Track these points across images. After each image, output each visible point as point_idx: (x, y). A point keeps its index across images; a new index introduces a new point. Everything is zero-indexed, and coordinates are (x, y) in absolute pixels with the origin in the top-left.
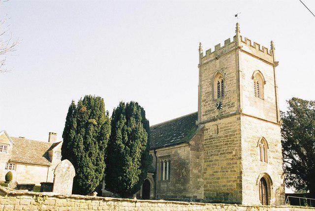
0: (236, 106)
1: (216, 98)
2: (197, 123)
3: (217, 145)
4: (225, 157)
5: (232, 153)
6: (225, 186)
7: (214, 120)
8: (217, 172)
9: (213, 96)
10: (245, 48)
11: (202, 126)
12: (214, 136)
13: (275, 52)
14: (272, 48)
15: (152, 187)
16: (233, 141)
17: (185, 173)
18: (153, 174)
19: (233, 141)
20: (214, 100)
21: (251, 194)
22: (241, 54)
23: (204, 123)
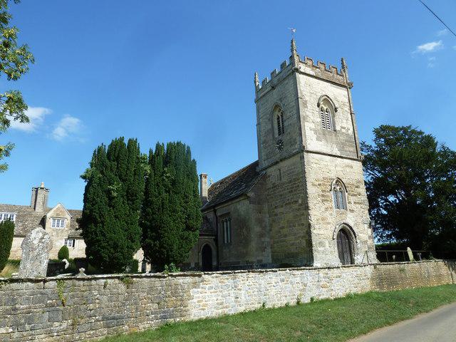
1: (277, 136)
5: (297, 202)
7: (277, 163)
9: (273, 135)
12: (277, 183)
15: (214, 253)
17: (245, 233)
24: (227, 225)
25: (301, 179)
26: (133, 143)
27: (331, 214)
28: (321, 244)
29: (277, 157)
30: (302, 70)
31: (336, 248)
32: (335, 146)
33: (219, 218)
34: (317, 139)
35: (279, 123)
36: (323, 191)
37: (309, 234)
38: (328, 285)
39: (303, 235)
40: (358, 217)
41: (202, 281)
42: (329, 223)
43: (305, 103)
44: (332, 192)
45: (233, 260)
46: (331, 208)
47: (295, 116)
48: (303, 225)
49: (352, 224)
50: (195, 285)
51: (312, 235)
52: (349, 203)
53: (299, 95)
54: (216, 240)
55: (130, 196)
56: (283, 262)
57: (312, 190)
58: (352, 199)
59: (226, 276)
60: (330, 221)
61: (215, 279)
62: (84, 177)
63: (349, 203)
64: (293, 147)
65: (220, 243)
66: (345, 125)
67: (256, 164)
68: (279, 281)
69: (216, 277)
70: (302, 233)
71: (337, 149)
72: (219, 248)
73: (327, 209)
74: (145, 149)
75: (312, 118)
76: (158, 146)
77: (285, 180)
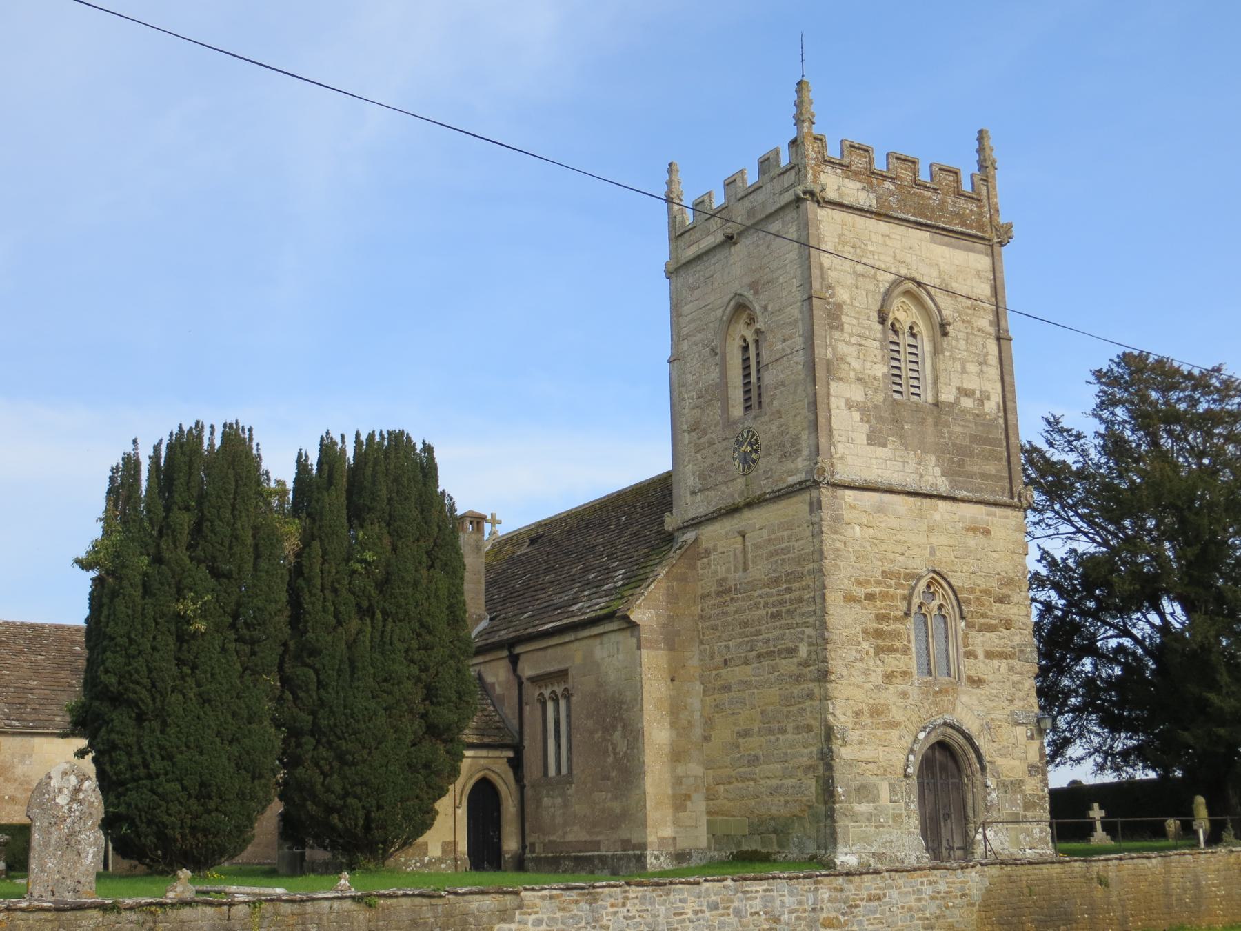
0: (805, 453)
1: (737, 411)
2: (671, 522)
3: (744, 617)
4: (774, 669)
5: (792, 651)
6: (774, 791)
7: (733, 510)
8: (746, 733)
9: (725, 409)
10: (832, 183)
11: (690, 536)
12: (735, 578)
13: (1001, 178)
14: (985, 166)
15: (509, 808)
16: (800, 600)
17: (622, 747)
18: (511, 754)
19: (800, 600)
20: (729, 423)
21: (881, 820)
22: (828, 223)
23: (696, 523)
24: (557, 711)
25: (808, 580)
26: (237, 444)
27: (904, 695)
28: (865, 792)
29: (734, 491)
30: (831, 194)
31: (914, 806)
32: (932, 459)
33: (526, 684)
34: (871, 440)
35: (746, 367)
36: (880, 618)
37: (826, 759)
38: (842, 919)
39: (806, 761)
40: (997, 705)
41: (520, 907)
42: (894, 725)
43: (834, 316)
44: (910, 623)
45: (576, 834)
46: (905, 674)
47: (800, 357)
48: (809, 728)
49: (971, 725)
50: (505, 916)
51: (837, 763)
52: (970, 655)
53: (816, 285)
54: (516, 764)
55: (238, 623)
56: (745, 848)
57: (845, 620)
58: (980, 642)
59: (574, 895)
60: (897, 715)
61: (547, 902)
62: (84, 564)
63: (970, 655)
64: (790, 465)
65: (532, 770)
66: (971, 383)
67: (654, 497)
68: (704, 908)
69: (551, 897)
70: (807, 754)
71: (938, 471)
72: (529, 792)
73: (889, 677)
74: (279, 468)
75: (856, 364)
76: (327, 448)
77: (758, 571)
